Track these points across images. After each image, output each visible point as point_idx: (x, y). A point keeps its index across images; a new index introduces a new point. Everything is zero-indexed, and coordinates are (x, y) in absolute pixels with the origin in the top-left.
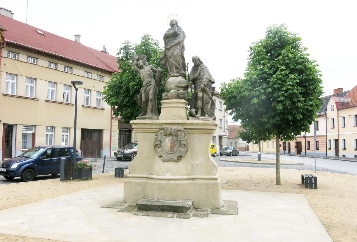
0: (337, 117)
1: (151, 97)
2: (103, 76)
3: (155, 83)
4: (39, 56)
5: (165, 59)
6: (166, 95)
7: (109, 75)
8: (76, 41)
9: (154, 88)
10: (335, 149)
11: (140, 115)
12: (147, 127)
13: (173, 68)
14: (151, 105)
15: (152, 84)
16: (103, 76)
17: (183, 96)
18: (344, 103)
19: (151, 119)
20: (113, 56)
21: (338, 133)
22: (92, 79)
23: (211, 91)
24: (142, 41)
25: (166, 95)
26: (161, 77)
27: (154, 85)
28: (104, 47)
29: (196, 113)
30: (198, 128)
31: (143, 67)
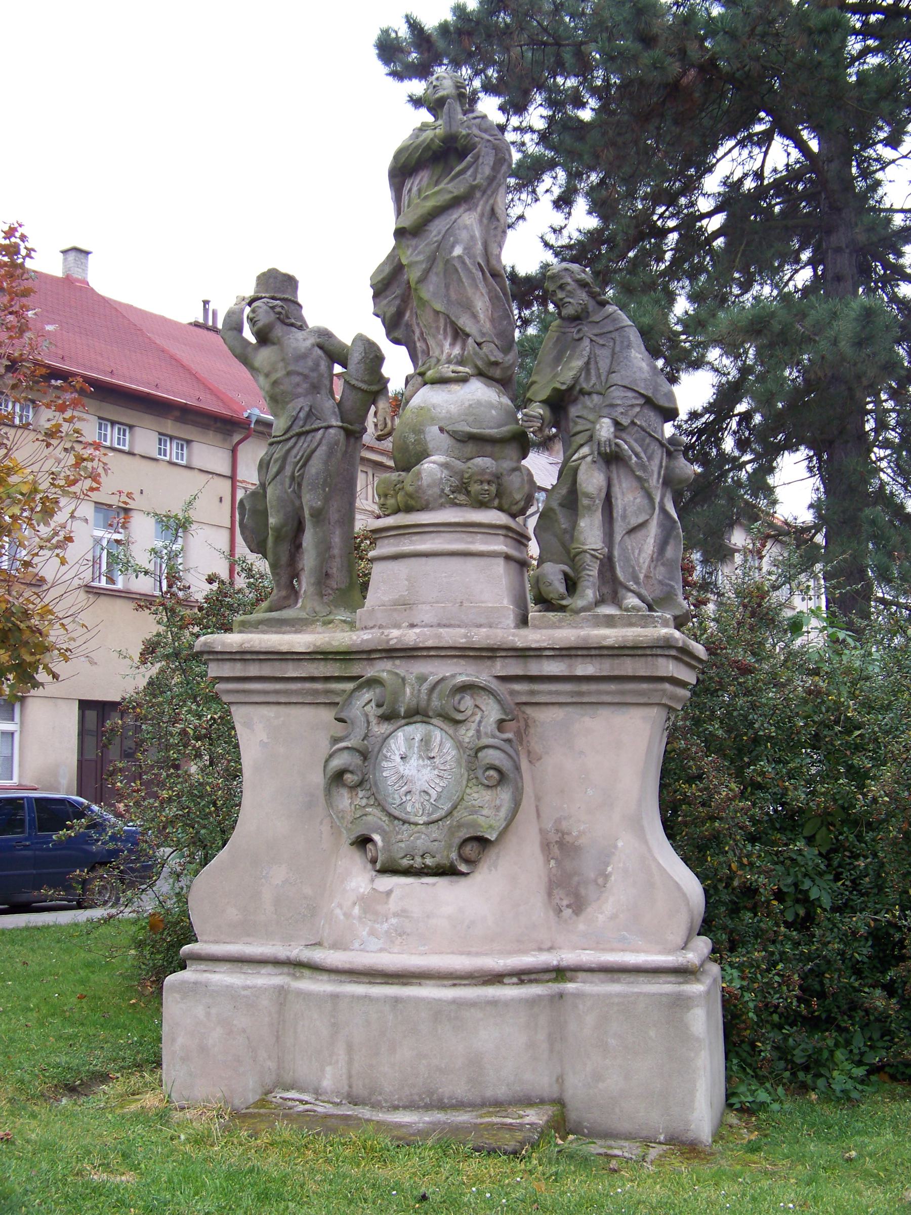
2: (189, 442)
3: (340, 424)
4: (129, 411)
7: (219, 436)
13: (441, 337)
16: (189, 442)
17: (493, 488)
20: (136, 309)
22: (133, 454)
23: (656, 462)
28: (206, 303)
29: (571, 585)
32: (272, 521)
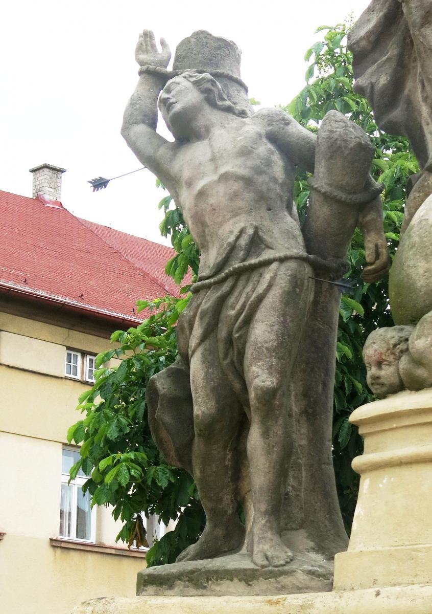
1: (260, 376)
5: (392, 50)
6: (401, 349)
8: (39, 200)
9: (292, 296)
11: (192, 548)
14: (268, 451)
15: (267, 263)
19: (261, 584)
24: (310, 73)
25: (401, 349)
26: (360, 197)
27: (292, 265)
30: (127, 555)
31: (201, 122)
32: (198, 410)
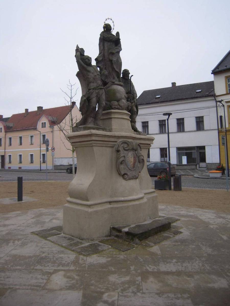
0: (4, 138)
10: (67, 164)
12: (106, 139)
18: (9, 126)
21: (5, 150)
